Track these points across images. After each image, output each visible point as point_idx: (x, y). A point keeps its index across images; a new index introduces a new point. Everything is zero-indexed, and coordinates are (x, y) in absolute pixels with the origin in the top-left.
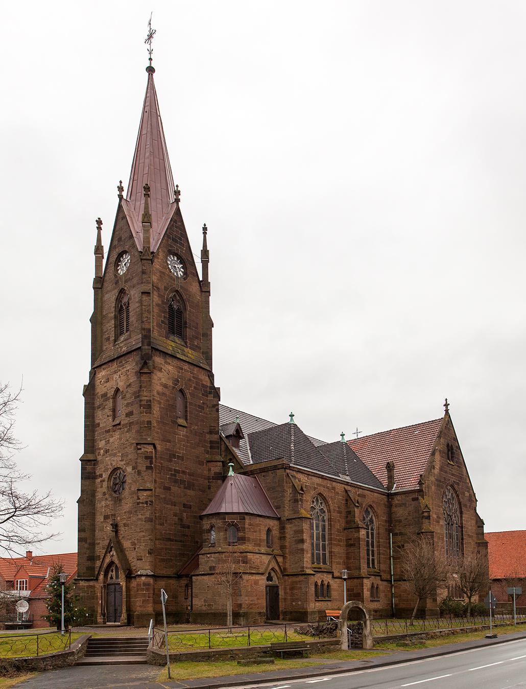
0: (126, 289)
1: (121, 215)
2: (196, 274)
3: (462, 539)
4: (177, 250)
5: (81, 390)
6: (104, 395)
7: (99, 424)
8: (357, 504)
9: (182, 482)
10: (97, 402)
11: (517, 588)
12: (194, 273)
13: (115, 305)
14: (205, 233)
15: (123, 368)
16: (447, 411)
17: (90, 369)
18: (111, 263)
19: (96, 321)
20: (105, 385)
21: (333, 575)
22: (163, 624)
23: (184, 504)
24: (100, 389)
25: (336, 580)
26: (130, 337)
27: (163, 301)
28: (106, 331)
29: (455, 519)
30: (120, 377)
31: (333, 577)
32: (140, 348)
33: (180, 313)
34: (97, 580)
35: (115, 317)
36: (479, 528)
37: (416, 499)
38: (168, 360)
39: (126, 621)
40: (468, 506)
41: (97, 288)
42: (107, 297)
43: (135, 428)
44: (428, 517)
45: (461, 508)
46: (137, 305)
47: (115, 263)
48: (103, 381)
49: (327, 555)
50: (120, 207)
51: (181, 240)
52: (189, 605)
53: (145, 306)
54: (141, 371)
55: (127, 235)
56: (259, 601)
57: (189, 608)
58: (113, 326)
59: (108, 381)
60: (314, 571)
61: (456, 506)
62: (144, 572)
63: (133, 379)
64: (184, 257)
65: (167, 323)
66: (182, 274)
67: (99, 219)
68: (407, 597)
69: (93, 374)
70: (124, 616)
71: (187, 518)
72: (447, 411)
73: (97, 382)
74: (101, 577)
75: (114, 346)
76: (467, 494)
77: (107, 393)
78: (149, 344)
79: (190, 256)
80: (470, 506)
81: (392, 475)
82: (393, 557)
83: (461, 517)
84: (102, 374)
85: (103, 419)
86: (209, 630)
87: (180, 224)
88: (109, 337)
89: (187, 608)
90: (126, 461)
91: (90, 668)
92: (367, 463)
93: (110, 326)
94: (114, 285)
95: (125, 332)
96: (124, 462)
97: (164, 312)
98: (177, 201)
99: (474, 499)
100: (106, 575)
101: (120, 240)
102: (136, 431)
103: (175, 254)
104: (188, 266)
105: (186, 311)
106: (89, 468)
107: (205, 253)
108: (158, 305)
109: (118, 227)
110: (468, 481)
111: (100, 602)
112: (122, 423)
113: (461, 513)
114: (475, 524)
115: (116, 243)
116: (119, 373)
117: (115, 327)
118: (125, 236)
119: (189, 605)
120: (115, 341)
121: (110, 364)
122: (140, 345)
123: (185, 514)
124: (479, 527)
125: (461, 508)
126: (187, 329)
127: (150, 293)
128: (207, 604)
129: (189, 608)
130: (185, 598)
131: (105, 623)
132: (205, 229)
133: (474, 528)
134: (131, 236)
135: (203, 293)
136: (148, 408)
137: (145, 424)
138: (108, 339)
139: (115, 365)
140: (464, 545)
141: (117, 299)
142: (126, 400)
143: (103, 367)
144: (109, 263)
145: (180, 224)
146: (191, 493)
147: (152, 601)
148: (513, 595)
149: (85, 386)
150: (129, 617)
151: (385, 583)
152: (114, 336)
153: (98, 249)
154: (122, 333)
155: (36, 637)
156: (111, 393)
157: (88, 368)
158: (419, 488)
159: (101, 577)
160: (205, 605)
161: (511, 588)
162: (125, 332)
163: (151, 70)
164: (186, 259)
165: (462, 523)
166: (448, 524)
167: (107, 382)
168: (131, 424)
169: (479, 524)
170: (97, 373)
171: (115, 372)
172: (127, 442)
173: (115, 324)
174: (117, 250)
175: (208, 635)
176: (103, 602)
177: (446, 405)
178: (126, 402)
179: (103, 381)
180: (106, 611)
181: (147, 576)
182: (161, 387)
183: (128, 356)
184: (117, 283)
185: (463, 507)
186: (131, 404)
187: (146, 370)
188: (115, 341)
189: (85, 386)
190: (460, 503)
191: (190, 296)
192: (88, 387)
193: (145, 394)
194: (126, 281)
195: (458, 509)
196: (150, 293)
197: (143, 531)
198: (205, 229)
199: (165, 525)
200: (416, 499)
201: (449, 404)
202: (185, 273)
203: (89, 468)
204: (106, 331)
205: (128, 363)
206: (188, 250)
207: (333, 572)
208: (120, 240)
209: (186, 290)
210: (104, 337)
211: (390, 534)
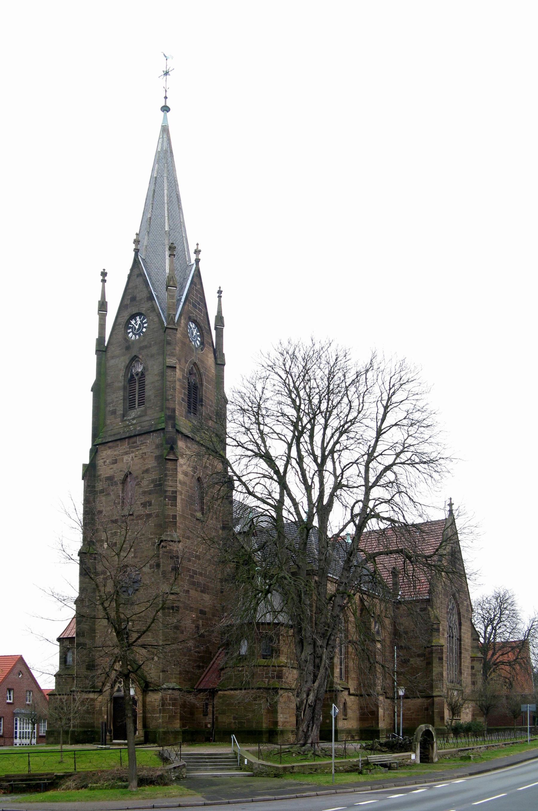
1: (136, 272)
3: (460, 653)
4: (196, 316)
5: (79, 472)
7: (100, 512)
8: (372, 615)
9: (199, 584)
10: (100, 486)
11: (531, 705)
14: (220, 297)
15: (138, 450)
16: (451, 511)
18: (120, 324)
20: (112, 466)
21: (349, 692)
25: (352, 697)
27: (183, 375)
30: (132, 459)
31: (350, 694)
32: (163, 429)
35: (124, 388)
37: (423, 610)
38: (189, 445)
39: (142, 739)
42: (112, 362)
44: (438, 630)
45: (460, 619)
46: (157, 378)
47: (125, 325)
48: (108, 461)
49: (343, 670)
50: (136, 262)
52: (210, 723)
54: (167, 458)
55: (145, 295)
58: (121, 398)
59: (115, 462)
61: (456, 617)
63: (151, 463)
64: (202, 325)
65: (187, 401)
66: (199, 344)
68: (411, 716)
69: (94, 452)
72: (451, 511)
73: (100, 462)
74: (107, 688)
75: (122, 421)
79: (207, 323)
82: (397, 672)
83: (460, 629)
87: (199, 287)
88: (116, 409)
89: (206, 726)
90: (140, 558)
94: (124, 350)
96: (138, 560)
97: (184, 388)
100: (112, 687)
101: (133, 299)
104: (205, 334)
105: (202, 386)
106: (90, 562)
107: (220, 319)
108: (179, 380)
109: (131, 285)
110: (466, 589)
111: (106, 717)
112: (135, 514)
113: (460, 624)
115: (127, 302)
117: (124, 399)
118: (142, 295)
119: (210, 723)
120: (124, 416)
121: (119, 443)
125: (460, 619)
127: (175, 367)
128: (237, 721)
131: (111, 740)
132: (220, 292)
133: (470, 641)
134: (151, 298)
137: (170, 519)
138: (114, 412)
142: (140, 487)
144: (117, 324)
146: (206, 597)
148: (527, 712)
149: (84, 465)
151: (389, 701)
152: (122, 409)
154: (132, 407)
156: (119, 477)
157: (89, 445)
159: (107, 688)
160: (235, 723)
161: (525, 705)
163: (166, 98)
165: (460, 636)
166: (450, 636)
168: (149, 516)
169: (475, 636)
170: (99, 450)
171: (126, 453)
173: (124, 396)
174: (129, 310)
175: (77, 767)
176: (109, 717)
177: (451, 505)
178: (141, 490)
181: (173, 689)
182: (183, 476)
183: (146, 436)
186: (150, 493)
187: (171, 457)
188: (124, 416)
189: (84, 465)
190: (459, 614)
192: (88, 467)
193: (170, 483)
194: (142, 348)
195: (457, 620)
196: (175, 367)
198: (220, 292)
201: (453, 504)
202: (202, 343)
204: (112, 402)
205: (145, 444)
206: (206, 317)
209: (202, 362)
211: (393, 647)
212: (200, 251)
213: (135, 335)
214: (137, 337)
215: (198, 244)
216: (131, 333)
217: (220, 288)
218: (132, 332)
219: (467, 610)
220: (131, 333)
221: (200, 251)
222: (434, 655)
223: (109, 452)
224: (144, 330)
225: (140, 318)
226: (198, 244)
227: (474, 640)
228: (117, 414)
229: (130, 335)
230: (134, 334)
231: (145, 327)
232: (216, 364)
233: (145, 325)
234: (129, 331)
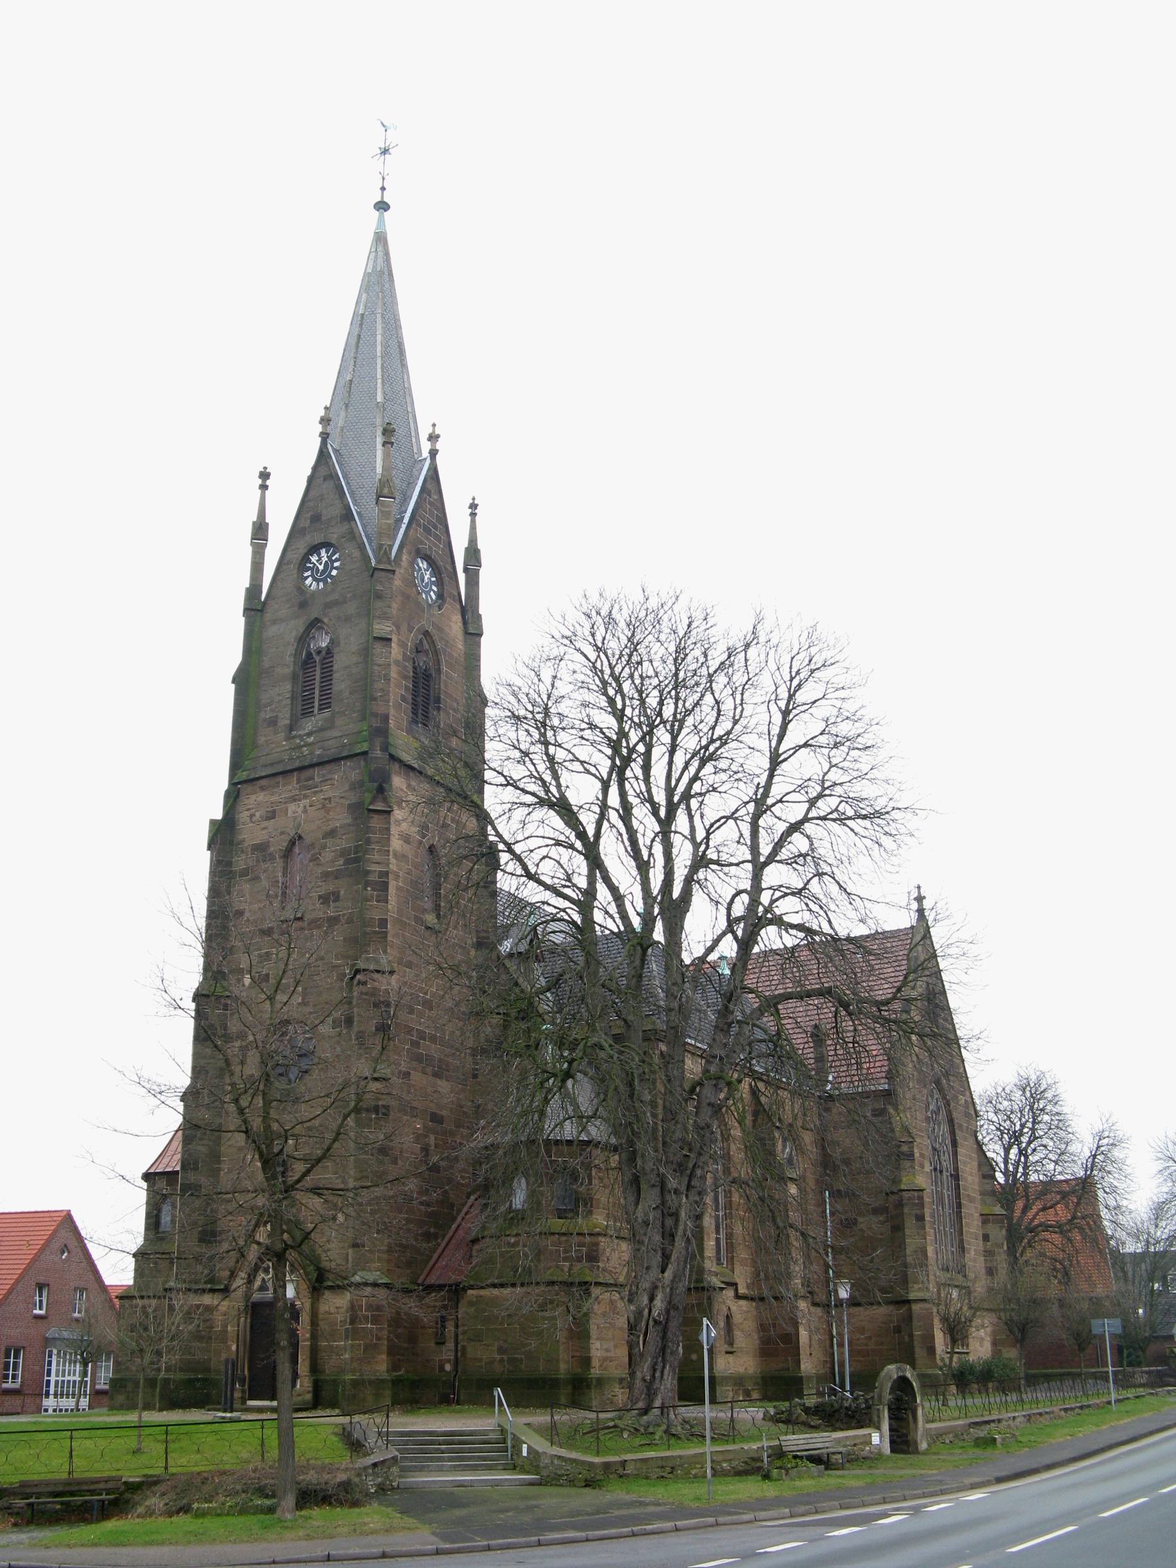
1: (323, 471)
3: (959, 1205)
7: (240, 913)
10: (240, 862)
12: (454, 596)
14: (473, 515)
15: (316, 792)
16: (921, 911)
17: (225, 785)
18: (289, 563)
19: (244, 680)
20: (265, 824)
22: (702, 1402)
23: (432, 1114)
24: (251, 832)
26: (330, 724)
27: (404, 654)
28: (269, 704)
32: (365, 753)
35: (294, 677)
38: (413, 783)
40: (965, 1128)
41: (253, 610)
43: (339, 934)
45: (953, 1133)
46: (355, 659)
47: (300, 564)
48: (258, 814)
50: (323, 455)
52: (449, 1361)
53: (379, 665)
54: (371, 807)
55: (337, 511)
57: (448, 1367)
58: (288, 695)
60: (723, 1282)
61: (944, 1128)
62: (371, 1277)
66: (434, 597)
67: (265, 468)
68: (867, 1345)
69: (233, 797)
71: (436, 1147)
72: (921, 911)
73: (243, 816)
76: (962, 1099)
77: (268, 842)
78: (385, 747)
79: (449, 560)
80: (967, 1127)
81: (825, 1052)
82: (832, 1248)
84: (255, 800)
85: (246, 898)
86: (72, 1430)
87: (436, 497)
89: (442, 1368)
91: (307, 1518)
92: (800, 1036)
94: (296, 608)
95: (316, 710)
96: (310, 1009)
100: (250, 1281)
102: (345, 940)
103: (427, 558)
104: (446, 580)
106: (215, 1013)
107: (473, 554)
108: (397, 662)
109: (312, 494)
111: (234, 1348)
119: (449, 1361)
120: (291, 728)
121: (280, 779)
122: (365, 747)
123: (432, 1137)
125: (953, 1133)
126: (441, 713)
127: (390, 640)
129: (448, 1367)
130: (437, 1343)
131: (244, 1402)
132: (473, 506)
133: (977, 1180)
134: (348, 516)
135: (470, 637)
136: (381, 891)
137: (374, 926)
138: (273, 722)
139: (290, 786)
140: (964, 1220)
146: (444, 1086)
147: (385, 1348)
149: (213, 822)
150: (317, 1387)
151: (819, 1311)
153: (260, 531)
154: (307, 712)
155: (69, 1433)
156: (278, 845)
157: (222, 782)
158: (886, 1087)
160: (502, 1360)
162: (316, 710)
164: (443, 569)
166: (935, 1169)
168: (333, 921)
169: (986, 1169)
170: (242, 793)
171: (294, 799)
172: (320, 963)
177: (920, 899)
179: (258, 814)
181: (375, 1285)
183: (333, 766)
184: (303, 605)
186: (337, 875)
187: (379, 806)
188: (291, 728)
189: (213, 822)
190: (951, 1121)
191: (447, 642)
194: (328, 606)
195: (947, 1135)
196: (390, 640)
197: (367, 1177)
198: (473, 506)
199: (399, 1162)
201: (924, 897)
203: (215, 1013)
205: (329, 782)
207: (736, 1284)
208: (316, 518)
209: (440, 629)
210: (262, 715)
211: (822, 1193)
212: (438, 436)
213: (318, 581)
214: (321, 585)
215: (434, 425)
216: (310, 578)
217: (474, 499)
218: (312, 576)
219: (967, 1115)
220: (310, 578)
221: (438, 436)
222: (906, 1210)
223: (261, 797)
224: (334, 573)
225: (327, 552)
226: (434, 425)
227: (984, 1177)
229: (309, 581)
230: (315, 579)
231: (336, 568)
232: (466, 633)
233: (336, 564)
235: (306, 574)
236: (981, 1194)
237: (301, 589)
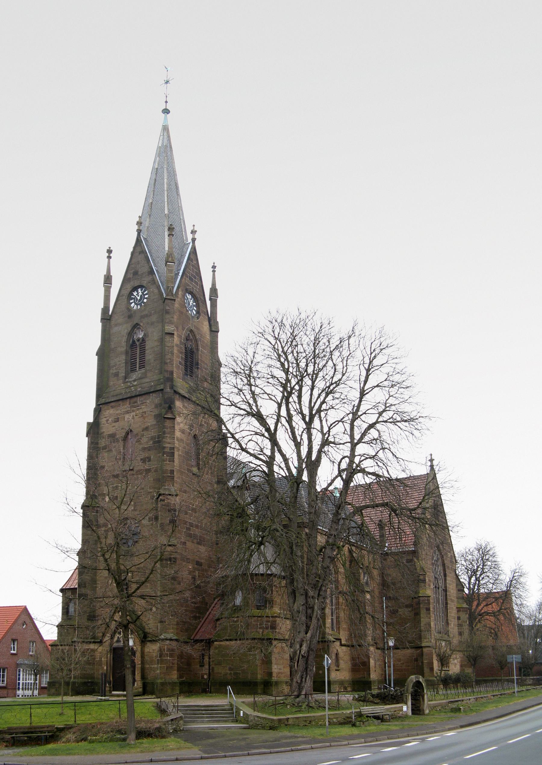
0: (141, 324)
2: (206, 313)
3: (447, 604)
6: (112, 436)
7: (103, 467)
10: (102, 443)
13: (127, 339)
15: (139, 409)
16: (432, 466)
17: (94, 405)
18: (123, 295)
20: (114, 424)
23: (197, 561)
24: (107, 428)
25: (343, 648)
26: (144, 376)
27: (181, 341)
28: (115, 366)
29: (441, 583)
32: (162, 390)
33: (192, 352)
34: (101, 642)
35: (127, 353)
36: (460, 592)
37: (410, 561)
38: (186, 405)
39: (141, 690)
40: (450, 568)
45: (444, 570)
48: (110, 420)
50: (138, 241)
51: (195, 278)
52: (206, 674)
54: (165, 416)
55: (146, 269)
56: (285, 669)
57: (205, 677)
58: (124, 361)
59: (117, 420)
60: (334, 638)
63: (151, 421)
66: (195, 313)
67: (110, 248)
68: (402, 667)
69: (98, 411)
70: (138, 684)
72: (432, 466)
73: (103, 421)
75: (124, 382)
79: (202, 294)
81: (384, 533)
82: (386, 623)
83: (445, 580)
87: (195, 262)
88: (118, 372)
89: (203, 677)
90: (140, 511)
92: (372, 525)
93: (119, 361)
98: (194, 240)
99: (454, 561)
100: (112, 638)
104: (201, 304)
105: (198, 351)
106: (92, 515)
107: (214, 291)
108: (177, 345)
109: (133, 261)
110: (449, 541)
111: (105, 668)
112: (135, 469)
113: (445, 575)
114: (455, 588)
115: (130, 276)
116: (132, 414)
119: (206, 674)
120: (126, 378)
121: (120, 402)
123: (197, 572)
124: (459, 590)
125: (444, 570)
127: (173, 334)
129: (205, 677)
130: (200, 666)
131: (110, 692)
132: (214, 267)
137: (168, 473)
139: (126, 406)
141: (129, 333)
142: (140, 444)
143: (112, 404)
144: (121, 295)
145: (195, 262)
146: (202, 549)
149: (89, 424)
150: (145, 686)
151: (379, 651)
153: (108, 279)
154: (133, 370)
155: (30, 706)
156: (121, 434)
157: (93, 404)
158: (413, 549)
159: (107, 638)
160: (231, 674)
164: (199, 299)
167: (115, 422)
168: (148, 471)
169: (460, 587)
170: (103, 409)
171: (128, 412)
174: (132, 283)
176: (109, 668)
177: (431, 460)
178: (141, 446)
179: (110, 420)
180: (111, 679)
181: (171, 640)
182: (180, 433)
185: (446, 569)
186: (149, 449)
187: (169, 416)
188: (126, 378)
189: (89, 424)
190: (444, 565)
192: (92, 425)
194: (142, 317)
195: (442, 571)
196: (173, 334)
197: (167, 591)
198: (214, 267)
200: (410, 561)
201: (434, 460)
204: (115, 366)
205: (145, 404)
207: (341, 639)
208: (136, 273)
209: (198, 329)
211: (382, 598)
212: (196, 231)
213: (137, 305)
214: (139, 307)
217: (214, 263)
218: (134, 302)
219: (451, 562)
221: (196, 231)
223: (112, 411)
224: (145, 300)
227: (459, 590)
228: (120, 376)
229: (133, 305)
230: (136, 304)
231: (146, 298)
232: (211, 331)
233: (146, 296)
234: (131, 301)
235: (131, 301)
236: (457, 598)
237: (129, 309)
